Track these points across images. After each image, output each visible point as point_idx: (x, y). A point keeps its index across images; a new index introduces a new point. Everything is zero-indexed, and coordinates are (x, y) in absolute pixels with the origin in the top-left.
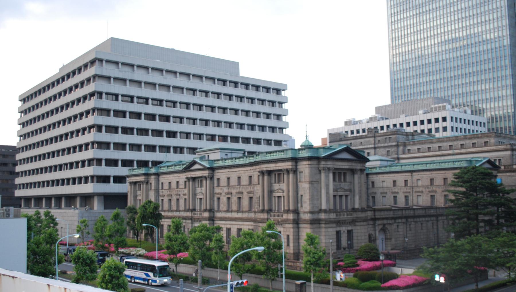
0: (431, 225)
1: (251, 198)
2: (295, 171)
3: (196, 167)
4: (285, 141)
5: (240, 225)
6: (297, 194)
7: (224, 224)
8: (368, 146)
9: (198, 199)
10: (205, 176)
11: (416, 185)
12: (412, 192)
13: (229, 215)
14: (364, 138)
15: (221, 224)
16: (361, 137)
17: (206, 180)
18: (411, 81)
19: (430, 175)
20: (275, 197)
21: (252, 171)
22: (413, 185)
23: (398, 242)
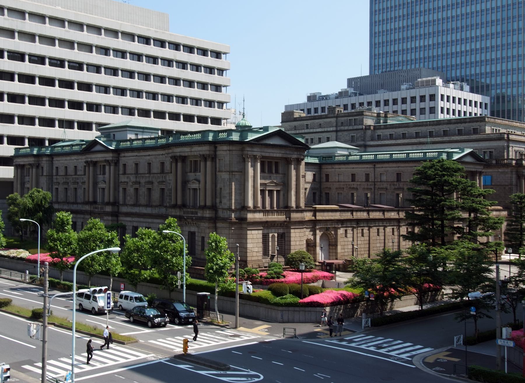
0: (391, 231)
1: (163, 190)
2: (214, 158)
3: (98, 148)
4: (224, 119)
5: (149, 223)
6: (216, 186)
7: (130, 221)
8: (329, 129)
9: (99, 188)
10: (108, 161)
11: (379, 180)
12: (374, 190)
13: (136, 210)
14: (324, 118)
15: (127, 221)
16: (320, 117)
17: (110, 166)
18: (401, 45)
19: (397, 169)
20: (190, 189)
21: (164, 156)
22: (376, 180)
23: (346, 250)
